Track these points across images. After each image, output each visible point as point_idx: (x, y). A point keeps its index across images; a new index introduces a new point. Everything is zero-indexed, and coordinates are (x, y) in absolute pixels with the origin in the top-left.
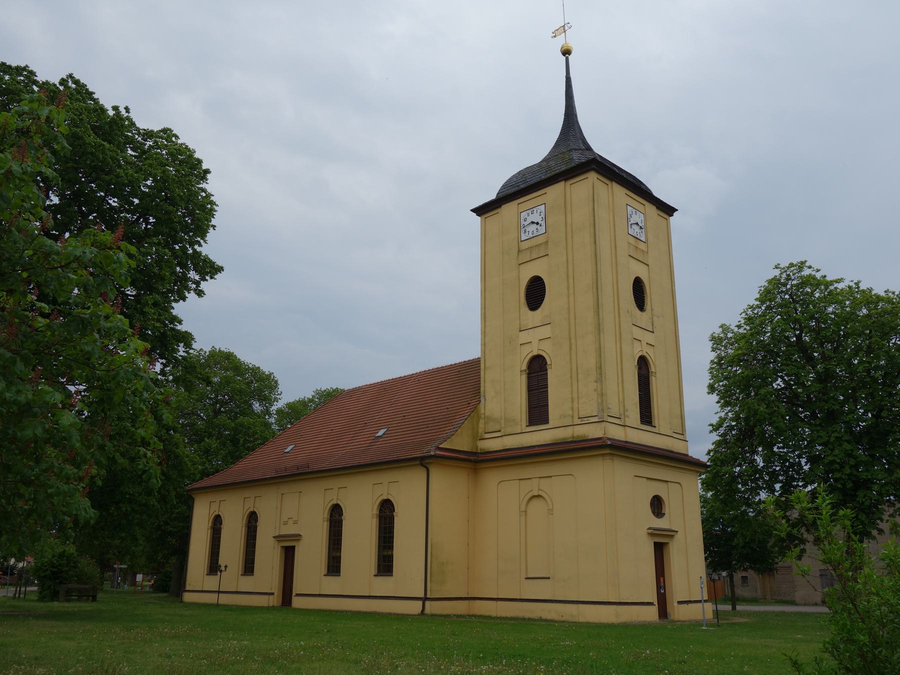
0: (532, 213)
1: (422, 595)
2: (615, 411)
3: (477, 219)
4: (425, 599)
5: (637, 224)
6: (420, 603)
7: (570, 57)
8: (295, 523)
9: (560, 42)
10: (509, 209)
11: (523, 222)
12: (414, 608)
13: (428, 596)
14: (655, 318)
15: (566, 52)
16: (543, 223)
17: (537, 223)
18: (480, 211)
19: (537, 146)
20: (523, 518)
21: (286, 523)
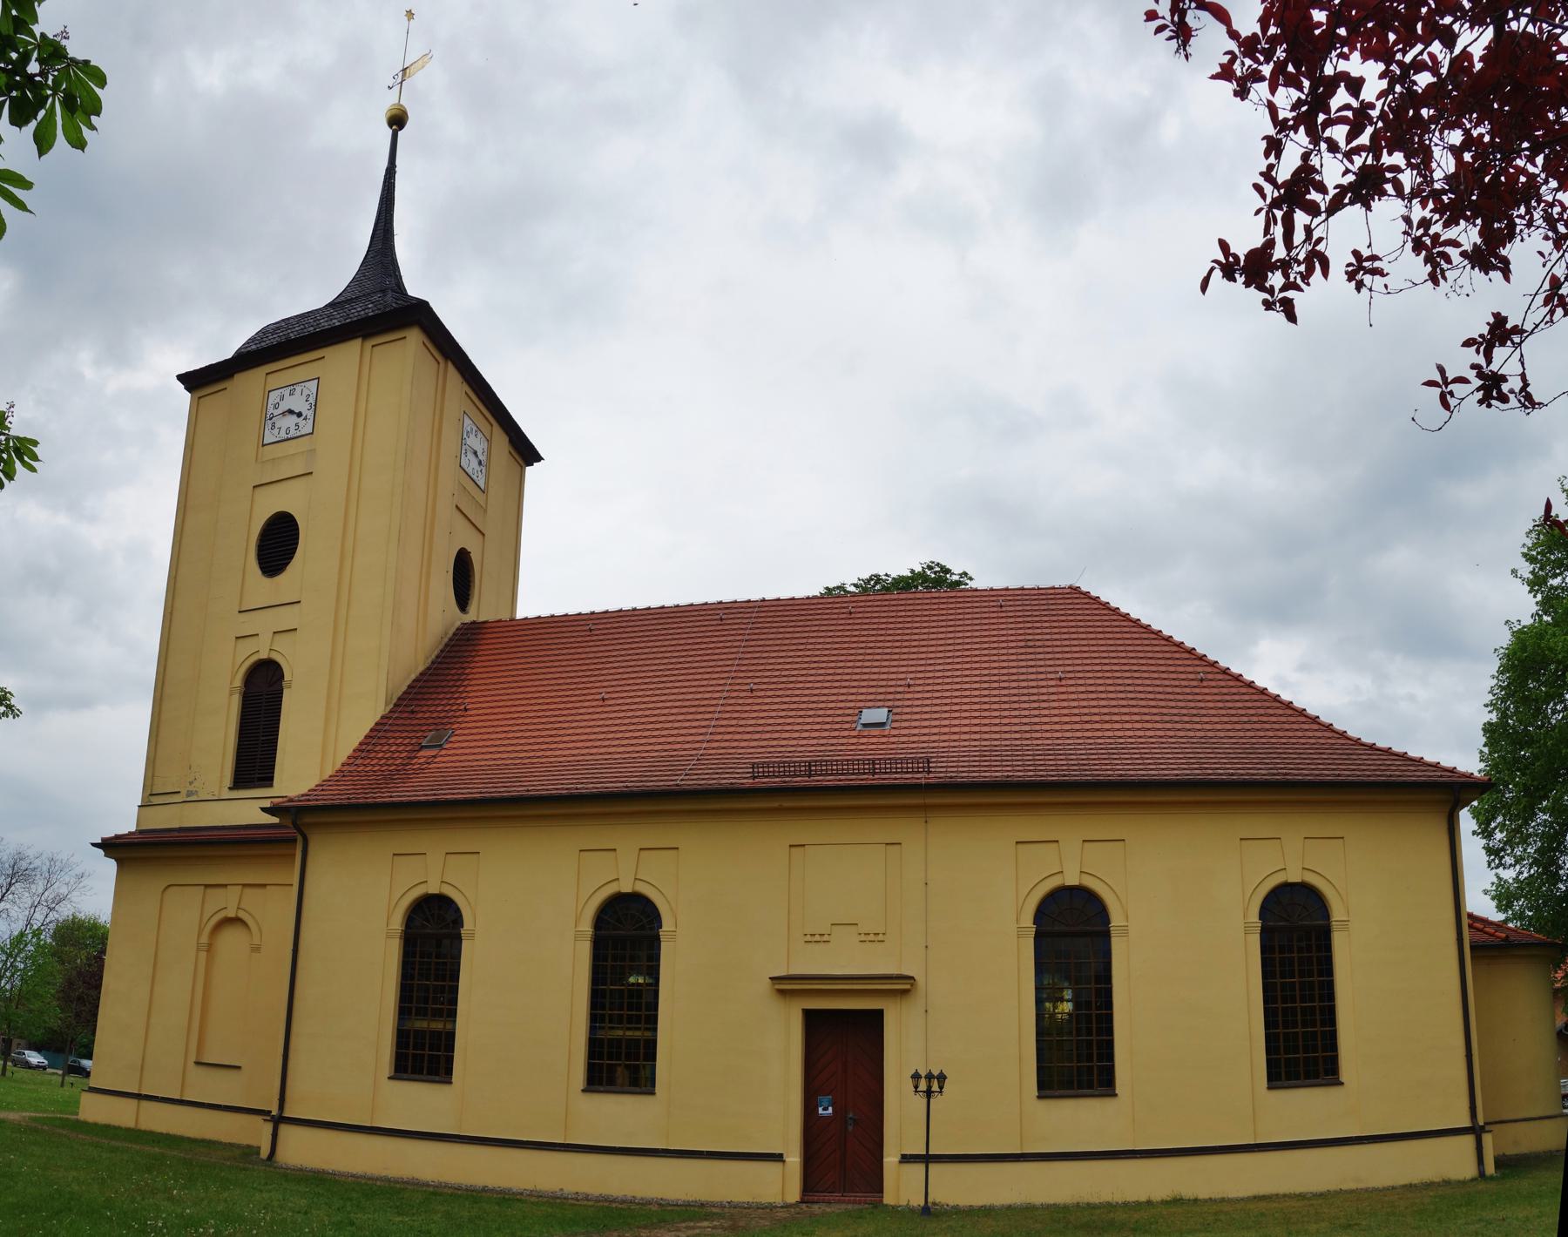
0: (290, 389)
3: (184, 397)
5: (475, 453)
8: (876, 938)
9: (388, 101)
10: (250, 382)
11: (270, 407)
15: (397, 121)
16: (310, 414)
17: (299, 415)
18: (191, 380)
19: (319, 285)
20: (203, 955)
21: (817, 939)
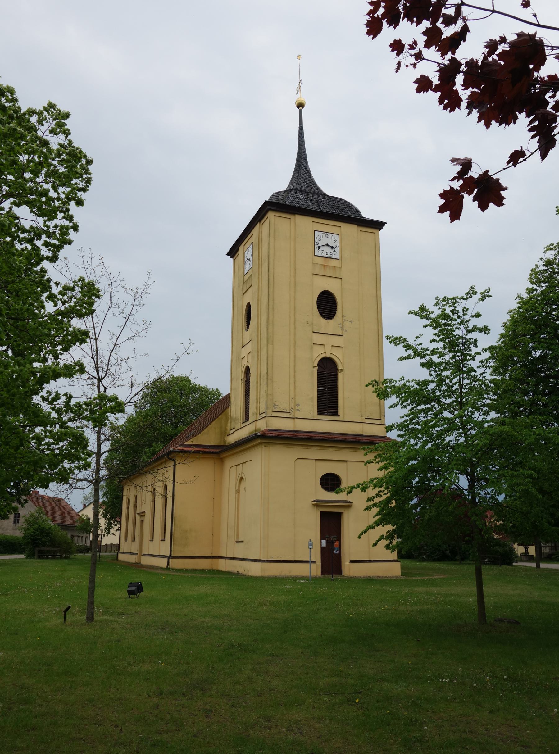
1: (168, 555)
2: (284, 405)
4: (169, 557)
6: (166, 560)
7: (303, 110)
12: (163, 563)
13: (172, 555)
14: (346, 323)
15: (300, 106)
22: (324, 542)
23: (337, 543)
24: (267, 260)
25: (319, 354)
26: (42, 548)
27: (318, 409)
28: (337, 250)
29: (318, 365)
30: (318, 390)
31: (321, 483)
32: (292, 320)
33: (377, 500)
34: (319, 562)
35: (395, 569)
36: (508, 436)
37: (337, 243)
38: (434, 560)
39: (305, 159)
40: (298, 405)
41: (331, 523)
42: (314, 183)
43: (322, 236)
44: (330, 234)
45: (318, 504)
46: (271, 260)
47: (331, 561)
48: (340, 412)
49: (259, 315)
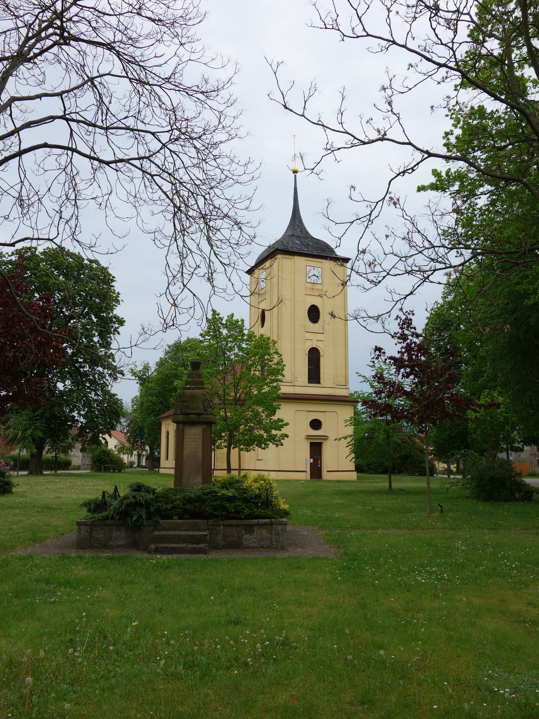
22: (312, 460)
23: (319, 461)
24: (277, 286)
25: (309, 345)
26: (106, 465)
27: (309, 380)
28: (320, 278)
29: (308, 352)
30: (309, 368)
31: (310, 425)
32: (293, 325)
33: (351, 443)
34: (309, 472)
35: (354, 476)
36: (274, 559)
37: (320, 274)
38: (379, 473)
39: (298, 211)
40: (297, 378)
41: (316, 449)
42: (304, 228)
43: (311, 269)
44: (317, 268)
45: (308, 437)
46: (280, 287)
47: (316, 471)
48: (322, 381)
49: (271, 320)
